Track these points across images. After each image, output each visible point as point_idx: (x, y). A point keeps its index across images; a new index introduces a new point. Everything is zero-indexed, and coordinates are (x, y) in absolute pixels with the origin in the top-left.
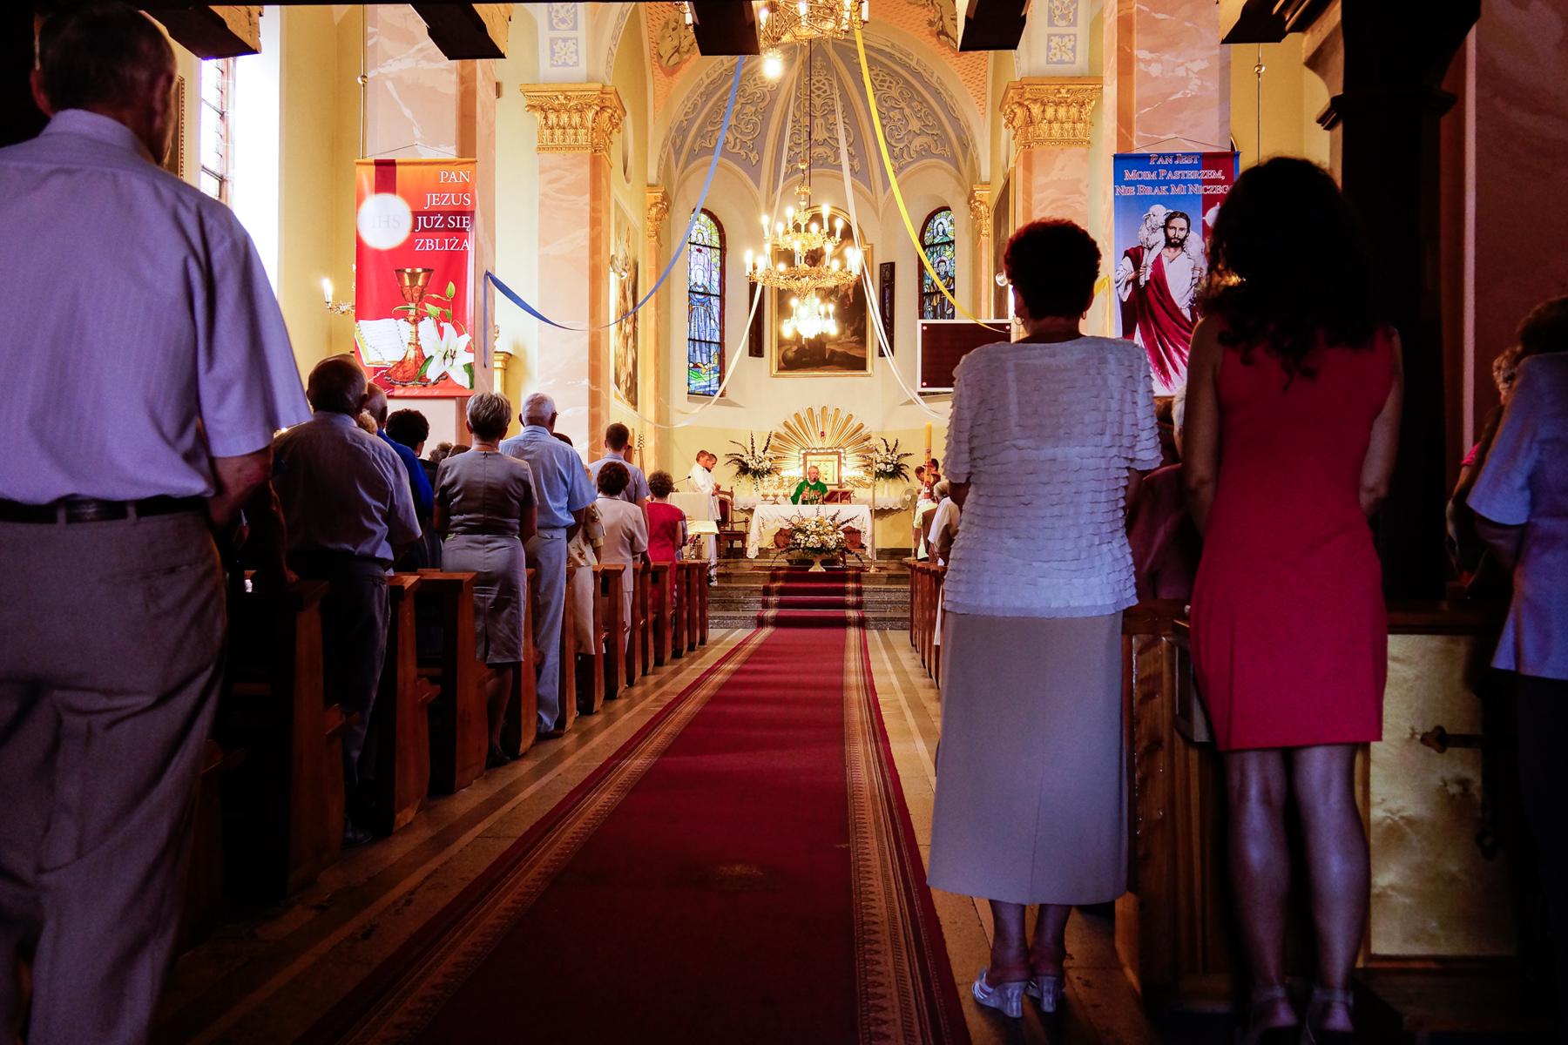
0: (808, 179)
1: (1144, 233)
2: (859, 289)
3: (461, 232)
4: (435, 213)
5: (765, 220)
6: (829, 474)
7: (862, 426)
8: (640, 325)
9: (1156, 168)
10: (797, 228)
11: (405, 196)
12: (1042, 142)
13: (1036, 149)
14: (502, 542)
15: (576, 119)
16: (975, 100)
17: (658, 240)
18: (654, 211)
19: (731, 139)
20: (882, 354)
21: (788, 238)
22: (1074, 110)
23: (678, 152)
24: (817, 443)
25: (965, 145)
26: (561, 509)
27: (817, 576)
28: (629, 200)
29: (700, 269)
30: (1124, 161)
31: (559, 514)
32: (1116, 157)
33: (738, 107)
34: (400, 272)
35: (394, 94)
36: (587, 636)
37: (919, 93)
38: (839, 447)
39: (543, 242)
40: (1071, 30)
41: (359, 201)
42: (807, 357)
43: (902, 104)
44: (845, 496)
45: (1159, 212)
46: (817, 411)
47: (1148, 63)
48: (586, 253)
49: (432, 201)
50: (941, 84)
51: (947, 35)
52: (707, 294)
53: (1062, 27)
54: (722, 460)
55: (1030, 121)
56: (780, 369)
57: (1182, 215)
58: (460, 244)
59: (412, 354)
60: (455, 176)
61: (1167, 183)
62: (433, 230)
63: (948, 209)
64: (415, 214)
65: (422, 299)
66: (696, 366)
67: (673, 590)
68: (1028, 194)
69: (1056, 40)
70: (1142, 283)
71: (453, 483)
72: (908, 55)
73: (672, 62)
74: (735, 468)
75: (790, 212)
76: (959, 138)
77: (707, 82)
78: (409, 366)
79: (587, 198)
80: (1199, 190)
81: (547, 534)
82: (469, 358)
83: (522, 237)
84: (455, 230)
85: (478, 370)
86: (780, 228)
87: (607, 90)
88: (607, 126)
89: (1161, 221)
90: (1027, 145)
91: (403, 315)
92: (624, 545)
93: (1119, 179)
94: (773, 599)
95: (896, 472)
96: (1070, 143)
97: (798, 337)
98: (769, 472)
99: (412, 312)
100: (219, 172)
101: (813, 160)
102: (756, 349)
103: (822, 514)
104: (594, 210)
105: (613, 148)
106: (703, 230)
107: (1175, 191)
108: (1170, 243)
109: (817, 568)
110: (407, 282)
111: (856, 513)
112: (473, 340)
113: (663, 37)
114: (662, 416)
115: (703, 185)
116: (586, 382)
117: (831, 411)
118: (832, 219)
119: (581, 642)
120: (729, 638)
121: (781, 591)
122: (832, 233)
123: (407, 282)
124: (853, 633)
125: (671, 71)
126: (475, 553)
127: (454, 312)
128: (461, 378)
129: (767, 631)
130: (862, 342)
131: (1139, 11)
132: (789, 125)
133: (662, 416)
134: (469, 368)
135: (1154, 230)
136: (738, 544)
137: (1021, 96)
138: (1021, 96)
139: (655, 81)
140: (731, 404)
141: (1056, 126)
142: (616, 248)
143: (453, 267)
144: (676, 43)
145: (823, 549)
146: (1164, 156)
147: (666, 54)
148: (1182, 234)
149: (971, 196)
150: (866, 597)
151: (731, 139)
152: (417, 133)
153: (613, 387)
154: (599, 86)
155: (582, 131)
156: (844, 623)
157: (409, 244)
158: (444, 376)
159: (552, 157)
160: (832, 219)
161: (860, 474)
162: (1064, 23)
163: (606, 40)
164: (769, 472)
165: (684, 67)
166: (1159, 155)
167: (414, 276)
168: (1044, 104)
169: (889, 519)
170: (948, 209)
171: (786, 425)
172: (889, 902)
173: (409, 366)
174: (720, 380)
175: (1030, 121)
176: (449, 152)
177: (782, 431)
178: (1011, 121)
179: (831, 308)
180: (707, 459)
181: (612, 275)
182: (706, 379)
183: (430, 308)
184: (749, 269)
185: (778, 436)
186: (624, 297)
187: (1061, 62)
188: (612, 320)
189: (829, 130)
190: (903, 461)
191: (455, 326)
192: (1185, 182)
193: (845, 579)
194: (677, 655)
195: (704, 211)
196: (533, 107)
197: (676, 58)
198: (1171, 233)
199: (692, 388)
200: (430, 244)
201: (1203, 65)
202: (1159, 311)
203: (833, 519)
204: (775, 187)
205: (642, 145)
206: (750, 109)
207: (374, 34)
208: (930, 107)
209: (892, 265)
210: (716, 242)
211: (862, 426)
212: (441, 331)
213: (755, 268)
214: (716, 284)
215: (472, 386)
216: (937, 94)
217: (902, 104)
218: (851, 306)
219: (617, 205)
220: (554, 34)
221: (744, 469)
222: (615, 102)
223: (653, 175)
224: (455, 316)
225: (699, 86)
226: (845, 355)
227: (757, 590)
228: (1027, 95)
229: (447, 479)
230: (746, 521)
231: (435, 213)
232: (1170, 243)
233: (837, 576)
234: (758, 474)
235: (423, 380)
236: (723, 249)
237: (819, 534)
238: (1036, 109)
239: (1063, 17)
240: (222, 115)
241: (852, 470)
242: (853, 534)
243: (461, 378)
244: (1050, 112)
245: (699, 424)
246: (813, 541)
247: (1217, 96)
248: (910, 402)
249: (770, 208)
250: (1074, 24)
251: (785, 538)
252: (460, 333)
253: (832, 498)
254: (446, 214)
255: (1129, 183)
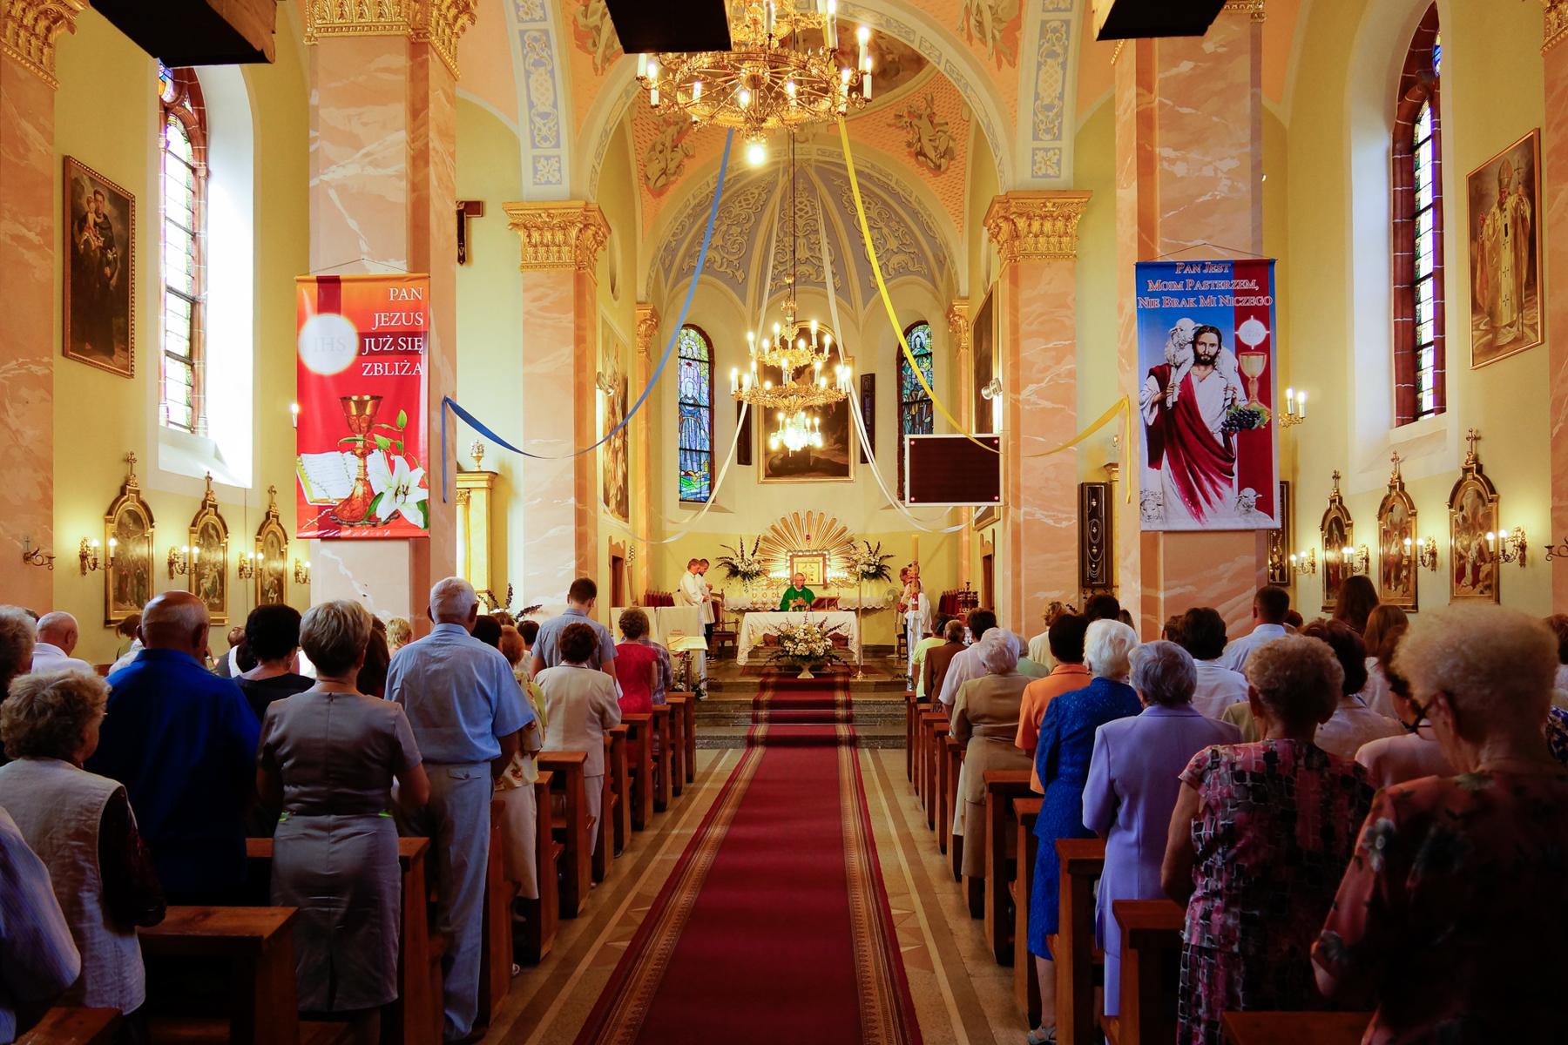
0: (793, 296)
1: (1170, 349)
2: (843, 406)
3: (413, 355)
4: (384, 335)
5: (750, 336)
6: (812, 572)
7: (845, 530)
8: (630, 439)
9: (1182, 278)
10: (784, 343)
11: (352, 316)
12: (1028, 255)
13: (1023, 263)
14: (360, 825)
15: (559, 237)
16: (952, 218)
17: (648, 355)
18: (643, 327)
19: (718, 259)
20: (864, 460)
21: (775, 355)
22: (1060, 224)
23: (667, 271)
24: (803, 546)
25: (941, 263)
26: (482, 735)
27: (806, 683)
28: (615, 317)
29: (690, 383)
30: (1147, 270)
31: (478, 743)
32: (1139, 266)
33: (724, 228)
34: (346, 400)
35: (338, 203)
36: (528, 875)
37: (896, 213)
38: (824, 549)
39: (528, 360)
40: (1057, 144)
41: (301, 321)
42: (790, 466)
43: (881, 224)
44: (831, 603)
45: (1187, 327)
46: (802, 515)
47: (1172, 161)
48: (571, 371)
49: (380, 321)
50: (920, 203)
51: (925, 156)
52: (697, 405)
53: (1047, 141)
54: (713, 564)
55: (1015, 235)
56: (767, 476)
57: (1212, 330)
58: (411, 368)
59: (360, 491)
60: (405, 293)
61: (1194, 294)
62: (382, 352)
63: (925, 323)
64: (363, 336)
65: (370, 430)
66: (687, 474)
67: (656, 719)
68: (1014, 308)
69: (1041, 154)
70: (1169, 404)
71: (281, 741)
72: (887, 175)
73: (659, 184)
74: (725, 571)
75: (777, 328)
76: (936, 256)
77: (693, 203)
78: (357, 503)
79: (571, 315)
80: (1231, 301)
81: (459, 772)
82: (423, 494)
83: (496, 360)
84: (406, 352)
85: (435, 507)
86: (766, 344)
87: (591, 207)
88: (590, 243)
89: (1190, 335)
90: (1013, 259)
91: (349, 447)
92: (592, 720)
93: (1142, 291)
94: (763, 713)
95: (878, 573)
96: (1055, 256)
97: (784, 449)
98: (757, 574)
99: (360, 444)
100: (191, 294)
101: (797, 278)
102: (744, 456)
103: (810, 621)
104: (579, 328)
105: (598, 266)
106: (692, 344)
107: (1208, 302)
108: (1199, 361)
109: (806, 675)
110: (354, 411)
111: (843, 621)
112: (428, 474)
113: (651, 160)
114: (655, 531)
115: (693, 300)
116: (572, 501)
117: (816, 516)
118: (820, 335)
119: (518, 884)
120: (720, 762)
121: (771, 705)
122: (820, 349)
123: (354, 411)
124: (845, 753)
125: (659, 193)
126: (317, 845)
127: (405, 445)
128: (414, 517)
129: (758, 752)
130: (845, 450)
131: (1162, 105)
132: (774, 244)
133: (655, 531)
134: (424, 506)
135: (1181, 346)
136: (728, 643)
137: (1007, 210)
138: (1007, 210)
139: (642, 202)
140: (723, 510)
141: (1042, 239)
142: (602, 365)
143: (404, 393)
144: (663, 165)
145: (811, 657)
146: (1191, 264)
147: (653, 176)
148: (1213, 351)
149: (950, 311)
150: (855, 711)
151: (718, 259)
152: (364, 248)
153: (601, 505)
154: (582, 203)
155: (565, 249)
156: (834, 742)
157: (355, 369)
158: (396, 515)
159: (535, 275)
160: (820, 335)
161: (844, 574)
162: (1048, 137)
163: (590, 159)
164: (757, 574)
165: (672, 188)
166: (1186, 264)
167: (361, 405)
168: (1029, 218)
169: (873, 618)
170: (925, 323)
171: (773, 528)
172: (877, 968)
173: (357, 503)
174: (711, 487)
175: (1015, 235)
176: (399, 267)
177: (770, 534)
178: (995, 236)
179: (817, 421)
180: (698, 566)
181: (600, 394)
182: (696, 486)
183: (380, 440)
184: (735, 387)
185: (766, 539)
186: (613, 412)
187: (1046, 176)
188: (600, 437)
189: (811, 249)
190: (885, 562)
191: (407, 459)
192: (1215, 293)
193: (833, 687)
194: (660, 808)
195: (686, 326)
196: (516, 225)
197: (662, 180)
198: (1201, 349)
199: (684, 495)
200: (379, 369)
201: (1234, 164)
202: (1190, 437)
203: (821, 626)
204: (760, 305)
205: (629, 262)
206: (735, 230)
207: (316, 139)
208: (908, 227)
209: (873, 376)
210: (705, 355)
211: (845, 530)
212: (392, 465)
213: (740, 386)
214: (705, 396)
215: (427, 525)
216: (915, 214)
217: (881, 224)
218: (835, 418)
219: (604, 322)
220: (537, 152)
221: (734, 572)
222: (600, 220)
223: (641, 292)
224: (406, 448)
225: (686, 207)
226: (829, 462)
227: (746, 703)
228: (1013, 209)
229: (274, 735)
230: (737, 622)
231: (384, 335)
232: (1199, 361)
233: (825, 683)
234: (747, 576)
235: (373, 520)
236: (711, 362)
237: (806, 641)
238: (1022, 223)
239: (1047, 131)
240: (194, 236)
241: (836, 570)
242: (841, 641)
243: (414, 517)
244: (1036, 226)
245: (691, 531)
246: (802, 649)
247: (1249, 197)
248: (890, 507)
249: (755, 325)
250: (1059, 138)
251: (774, 642)
252: (413, 467)
253: (820, 604)
254: (395, 335)
255: (1153, 295)
